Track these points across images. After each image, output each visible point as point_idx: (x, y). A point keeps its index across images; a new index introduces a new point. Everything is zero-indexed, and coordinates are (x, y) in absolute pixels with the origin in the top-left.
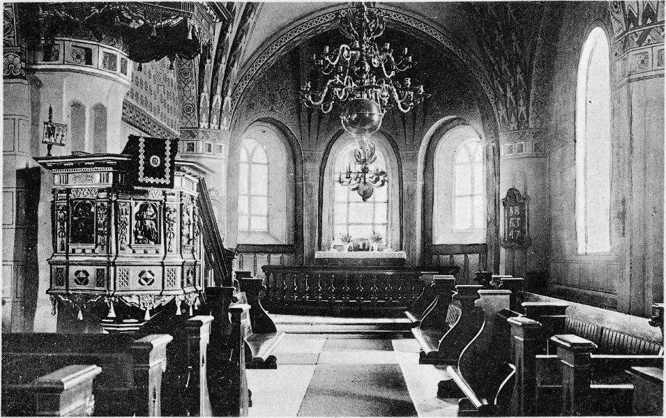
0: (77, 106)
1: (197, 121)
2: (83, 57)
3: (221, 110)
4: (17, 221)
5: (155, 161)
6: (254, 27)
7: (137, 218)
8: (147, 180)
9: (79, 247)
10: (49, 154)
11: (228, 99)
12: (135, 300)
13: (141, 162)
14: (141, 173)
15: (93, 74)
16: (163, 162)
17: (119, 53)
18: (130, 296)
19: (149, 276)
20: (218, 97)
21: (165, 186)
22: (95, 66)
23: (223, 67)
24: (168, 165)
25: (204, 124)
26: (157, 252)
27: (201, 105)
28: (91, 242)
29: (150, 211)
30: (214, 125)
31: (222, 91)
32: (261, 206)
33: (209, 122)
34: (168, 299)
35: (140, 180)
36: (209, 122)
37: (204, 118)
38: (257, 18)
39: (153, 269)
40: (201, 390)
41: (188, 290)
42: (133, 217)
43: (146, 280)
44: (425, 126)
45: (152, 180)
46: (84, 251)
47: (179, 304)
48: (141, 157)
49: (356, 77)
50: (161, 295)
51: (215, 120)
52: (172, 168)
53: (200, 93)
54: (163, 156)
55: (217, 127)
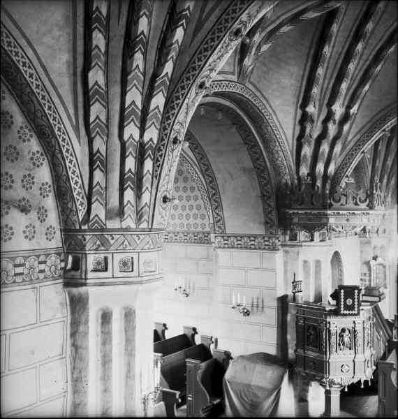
5: (349, 302)
7: (340, 336)
8: (345, 312)
13: (342, 303)
14: (342, 309)
15: (313, 246)
21: (355, 315)
24: (356, 303)
29: (347, 332)
35: (342, 312)
45: (348, 312)
47: (362, 382)
48: (342, 300)
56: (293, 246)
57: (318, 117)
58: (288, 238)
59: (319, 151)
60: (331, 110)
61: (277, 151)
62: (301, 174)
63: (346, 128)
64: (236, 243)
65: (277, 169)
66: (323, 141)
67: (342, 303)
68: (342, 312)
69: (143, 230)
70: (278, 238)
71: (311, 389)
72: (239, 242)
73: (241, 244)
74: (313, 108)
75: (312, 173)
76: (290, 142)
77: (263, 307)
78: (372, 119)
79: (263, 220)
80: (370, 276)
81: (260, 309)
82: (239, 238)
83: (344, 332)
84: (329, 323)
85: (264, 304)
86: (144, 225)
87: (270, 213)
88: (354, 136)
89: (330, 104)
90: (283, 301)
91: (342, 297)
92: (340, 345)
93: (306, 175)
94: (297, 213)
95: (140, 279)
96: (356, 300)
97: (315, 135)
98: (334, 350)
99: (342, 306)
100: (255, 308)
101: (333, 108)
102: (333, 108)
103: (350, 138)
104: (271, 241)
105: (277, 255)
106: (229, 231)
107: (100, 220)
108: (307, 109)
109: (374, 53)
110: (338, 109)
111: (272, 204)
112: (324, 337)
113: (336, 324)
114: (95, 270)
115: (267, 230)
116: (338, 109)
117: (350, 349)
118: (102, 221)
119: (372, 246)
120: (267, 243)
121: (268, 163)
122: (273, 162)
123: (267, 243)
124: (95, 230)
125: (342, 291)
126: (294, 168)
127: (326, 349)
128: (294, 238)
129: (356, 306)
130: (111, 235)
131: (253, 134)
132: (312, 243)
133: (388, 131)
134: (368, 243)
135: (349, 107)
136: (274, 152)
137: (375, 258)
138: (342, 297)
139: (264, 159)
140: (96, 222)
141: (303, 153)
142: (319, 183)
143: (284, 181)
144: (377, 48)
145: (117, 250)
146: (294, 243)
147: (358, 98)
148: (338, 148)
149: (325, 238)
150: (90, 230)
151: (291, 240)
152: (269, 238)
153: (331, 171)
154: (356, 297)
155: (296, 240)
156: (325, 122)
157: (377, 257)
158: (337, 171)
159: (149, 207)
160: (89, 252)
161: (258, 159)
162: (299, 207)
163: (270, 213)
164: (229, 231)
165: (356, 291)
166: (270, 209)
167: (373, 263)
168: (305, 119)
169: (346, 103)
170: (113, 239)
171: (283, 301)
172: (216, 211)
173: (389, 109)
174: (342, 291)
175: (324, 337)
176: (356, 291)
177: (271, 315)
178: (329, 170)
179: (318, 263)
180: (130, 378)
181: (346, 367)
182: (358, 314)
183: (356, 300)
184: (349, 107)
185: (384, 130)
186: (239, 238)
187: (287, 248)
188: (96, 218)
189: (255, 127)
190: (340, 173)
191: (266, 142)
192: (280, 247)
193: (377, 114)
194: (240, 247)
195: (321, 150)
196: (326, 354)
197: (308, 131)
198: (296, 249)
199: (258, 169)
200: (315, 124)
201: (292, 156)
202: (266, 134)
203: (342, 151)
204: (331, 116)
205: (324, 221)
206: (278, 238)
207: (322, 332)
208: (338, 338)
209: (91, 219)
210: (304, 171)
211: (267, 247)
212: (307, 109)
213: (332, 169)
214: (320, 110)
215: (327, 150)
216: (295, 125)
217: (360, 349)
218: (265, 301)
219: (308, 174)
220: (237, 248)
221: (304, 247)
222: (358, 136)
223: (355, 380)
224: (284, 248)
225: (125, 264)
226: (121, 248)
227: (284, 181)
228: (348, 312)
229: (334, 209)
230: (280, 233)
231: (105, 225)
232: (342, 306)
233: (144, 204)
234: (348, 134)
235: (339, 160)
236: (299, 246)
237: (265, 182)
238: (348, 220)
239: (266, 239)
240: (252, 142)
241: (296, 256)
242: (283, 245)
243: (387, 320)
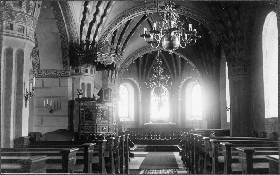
0: (83, 84)
1: (107, 82)
2: (85, 71)
4: (69, 115)
6: (125, 52)
7: (102, 114)
9: (87, 121)
10: (79, 97)
11: (117, 75)
12: (101, 135)
15: (88, 75)
17: (94, 69)
18: (100, 134)
19: (105, 128)
22: (88, 73)
25: (110, 83)
26: (107, 122)
27: (109, 77)
28: (90, 120)
34: (109, 134)
38: (126, 49)
39: (106, 127)
41: (114, 132)
42: (101, 113)
43: (104, 129)
46: (88, 122)
49: (158, 78)
50: (108, 133)
53: (108, 74)
55: (110, 83)
56: (77, 75)
58: (74, 71)
59: (91, 29)
60: (98, 9)
62: (82, 39)
63: (104, 19)
64: (46, 75)
65: (71, 34)
66: (94, 24)
69: (29, 16)
70: (69, 71)
72: (48, 74)
73: (48, 75)
74: (90, 7)
76: (78, 23)
77: (60, 107)
78: (116, 17)
79: (62, 61)
81: (59, 108)
82: (48, 72)
83: (104, 112)
84: (97, 106)
85: (62, 105)
86: (30, 14)
88: (108, 25)
90: (71, 104)
95: (27, 37)
100: (56, 108)
101: (99, 8)
104: (65, 73)
106: (42, 68)
107: (10, 6)
108: (87, 6)
111: (67, 53)
114: (6, 29)
115: (64, 67)
118: (11, 7)
120: (63, 74)
122: (69, 30)
123: (63, 74)
124: (7, 10)
126: (79, 36)
127: (95, 113)
128: (77, 71)
130: (15, 14)
131: (61, 13)
132: (87, 74)
135: (106, 10)
136: (70, 25)
139: (65, 29)
140: (8, 6)
141: (84, 29)
143: (74, 41)
145: (17, 21)
146: (78, 73)
147: (110, 6)
148: (100, 29)
150: (5, 9)
152: (65, 71)
155: (79, 72)
156: (95, 15)
159: (33, 6)
160: (4, 20)
161: (62, 28)
164: (42, 68)
166: (66, 55)
170: (16, 16)
171: (71, 104)
172: (35, 57)
173: (124, 14)
177: (65, 110)
178: (96, 40)
180: (20, 84)
181: (105, 128)
185: (121, 24)
186: (48, 72)
187: (74, 76)
188: (8, 5)
189: (62, 7)
191: (67, 18)
194: (48, 77)
195: (92, 29)
199: (62, 33)
200: (90, 14)
201: (79, 30)
202: (67, 14)
203: (102, 31)
206: (69, 71)
209: (6, 5)
210: (84, 38)
211: (63, 76)
212: (87, 6)
213: (97, 39)
214: (93, 8)
216: (81, 14)
218: (62, 104)
220: (47, 77)
222: (109, 25)
225: (20, 30)
226: (20, 21)
231: (13, 9)
233: (30, 4)
235: (100, 36)
236: (80, 75)
237: (64, 41)
240: (60, 17)
241: (78, 80)
242: (72, 75)
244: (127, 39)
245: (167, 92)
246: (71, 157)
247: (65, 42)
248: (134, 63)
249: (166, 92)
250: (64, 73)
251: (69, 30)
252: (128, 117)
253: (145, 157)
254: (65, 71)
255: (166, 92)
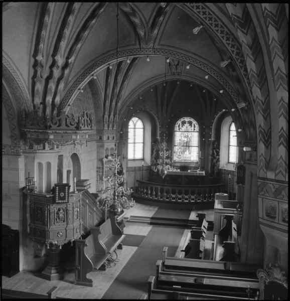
3: (114, 122)
5: (62, 194)
8: (59, 201)
12: (56, 242)
13: (57, 196)
14: (57, 199)
16: (65, 194)
20: (112, 116)
21: (66, 203)
23: (114, 103)
24: (67, 195)
29: (61, 211)
30: (111, 128)
31: (114, 113)
32: (139, 147)
33: (108, 127)
35: (57, 202)
36: (108, 127)
37: (106, 126)
40: (250, 13)
44: (216, 113)
45: (61, 201)
48: (57, 194)
51: (111, 126)
52: (68, 196)
54: (65, 193)
55: (111, 129)
57: (46, 63)
58: (27, 148)
61: (16, 87)
62: (35, 103)
63: (67, 71)
67: (57, 196)
68: (57, 202)
71: (131, 124)
74: (42, 58)
75: (44, 103)
76: (26, 80)
80: (103, 168)
87: (14, 129)
89: (54, 55)
91: (57, 192)
92: (56, 219)
93: (39, 103)
94: (32, 133)
96: (67, 193)
97: (45, 76)
98: (53, 223)
99: (57, 198)
102: (56, 58)
103: (70, 79)
105: (19, 159)
108: (37, 58)
109: (83, 22)
110: (60, 61)
112: (46, 215)
113: (54, 208)
116: (60, 61)
117: (64, 221)
119: (105, 148)
120: (13, 151)
121: (10, 95)
123: (13, 151)
125: (57, 188)
128: (31, 147)
129: (67, 197)
132: (44, 151)
133: (82, 89)
134: (102, 146)
135: (68, 58)
137: (107, 157)
138: (57, 192)
141: (36, 88)
142: (48, 111)
144: (84, 20)
148: (62, 86)
149: (54, 147)
151: (30, 148)
152: (14, 147)
153: (57, 101)
154: (67, 191)
156: (52, 67)
157: (108, 156)
158: (63, 100)
162: (31, 127)
163: (14, 129)
165: (67, 187)
167: (105, 160)
168: (36, 64)
169: (66, 55)
174: (57, 188)
175: (46, 215)
176: (67, 187)
179: (49, 164)
181: (61, 234)
182: (68, 202)
183: (67, 193)
184: (68, 58)
190: (64, 103)
192: (21, 154)
193: (88, 64)
195: (49, 87)
196: (47, 226)
197: (39, 73)
198: (32, 155)
203: (65, 87)
204: (55, 64)
205: (46, 137)
207: (45, 212)
208: (56, 215)
210: (38, 100)
212: (37, 58)
214: (47, 60)
215: (54, 87)
217: (70, 221)
219: (41, 103)
221: (38, 154)
223: (66, 242)
224: (25, 154)
227: (22, 108)
228: (61, 201)
229: (54, 129)
230: (21, 144)
232: (57, 198)
234: (69, 76)
235: (63, 94)
238: (62, 137)
239: (12, 148)
242: (24, 152)
243: (92, 194)
244: (123, 80)
245: (197, 126)
246: (254, 8)
247: (10, 110)
248: (152, 90)
249: (195, 127)
250: (13, 149)
251: (13, 94)
252: (143, 159)
253: (135, 249)
254: (14, 147)
255: (195, 127)
